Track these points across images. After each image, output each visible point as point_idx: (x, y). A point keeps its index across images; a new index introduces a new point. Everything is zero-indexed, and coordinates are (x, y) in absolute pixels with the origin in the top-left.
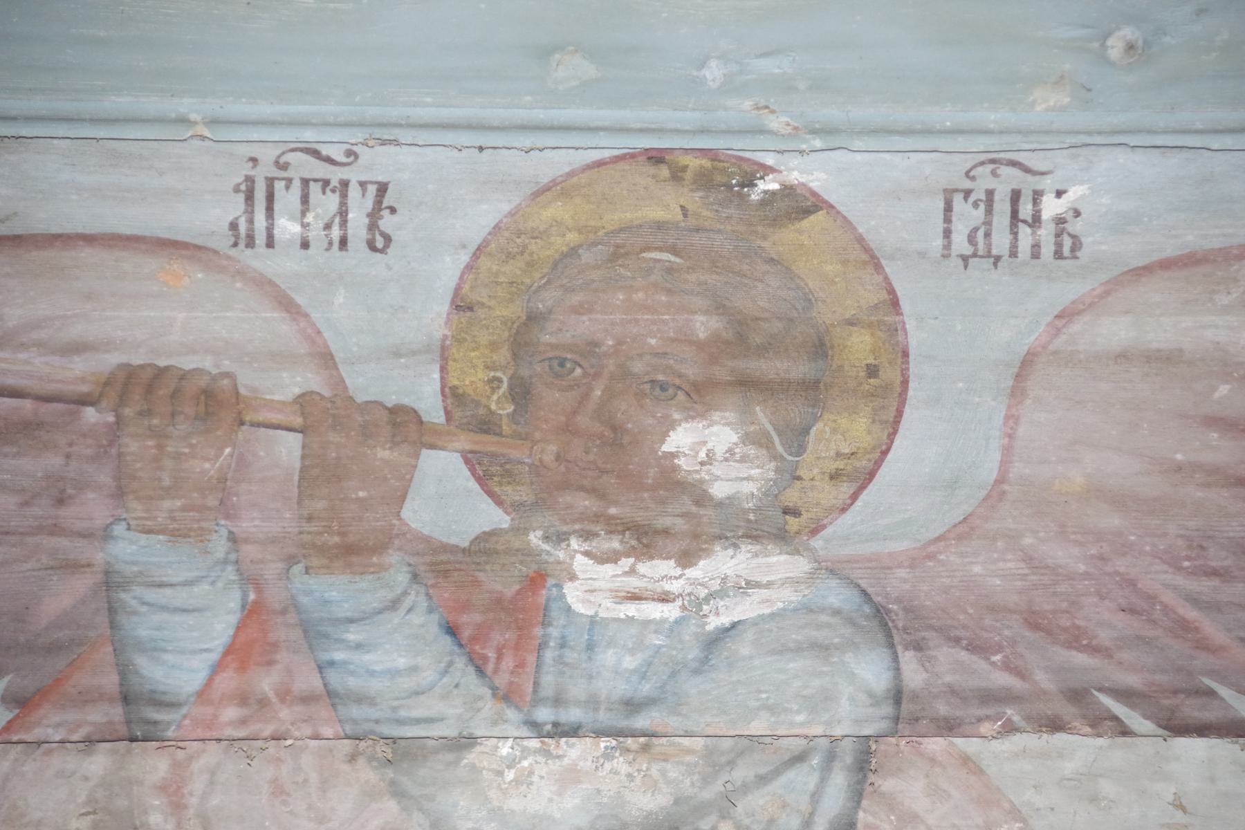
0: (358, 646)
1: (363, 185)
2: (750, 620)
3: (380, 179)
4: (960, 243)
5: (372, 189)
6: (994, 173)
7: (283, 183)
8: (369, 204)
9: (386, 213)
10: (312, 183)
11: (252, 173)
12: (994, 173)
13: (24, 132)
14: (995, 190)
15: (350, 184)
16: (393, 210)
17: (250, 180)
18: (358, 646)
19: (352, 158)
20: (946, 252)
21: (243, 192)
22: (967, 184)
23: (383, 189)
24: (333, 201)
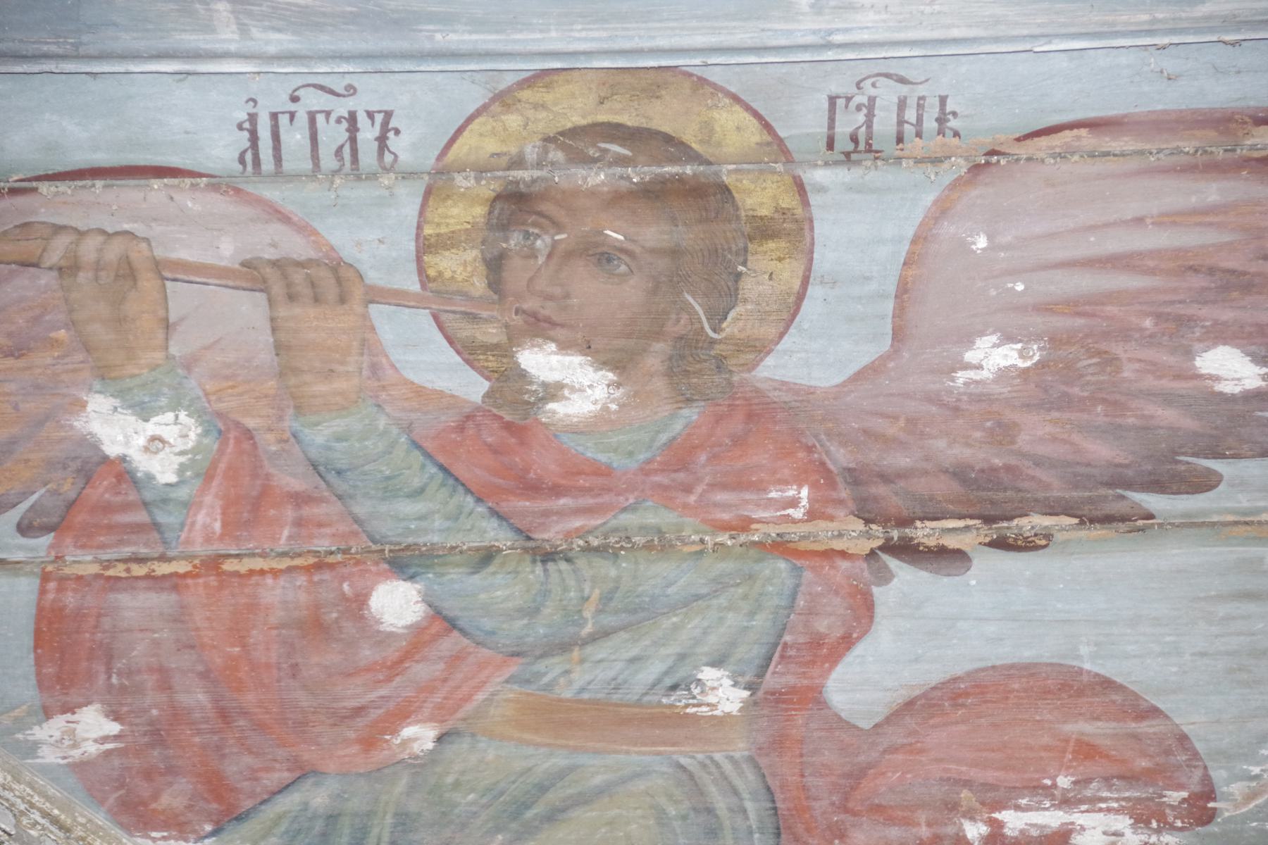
0: (313, 726)
1: (370, 115)
2: (404, 577)
3: (385, 108)
4: (328, 161)
5: (379, 118)
6: (874, 85)
7: (287, 116)
8: (377, 131)
9: (391, 135)
10: (280, 116)
11: (254, 111)
12: (874, 85)
13: (132, 68)
14: (296, 112)
15: (357, 114)
16: (397, 132)
17: (253, 118)
18: (313, 726)
19: (352, 91)
20: (921, 102)
21: (247, 130)
22: (292, 107)
23: (388, 115)
24: (341, 133)
